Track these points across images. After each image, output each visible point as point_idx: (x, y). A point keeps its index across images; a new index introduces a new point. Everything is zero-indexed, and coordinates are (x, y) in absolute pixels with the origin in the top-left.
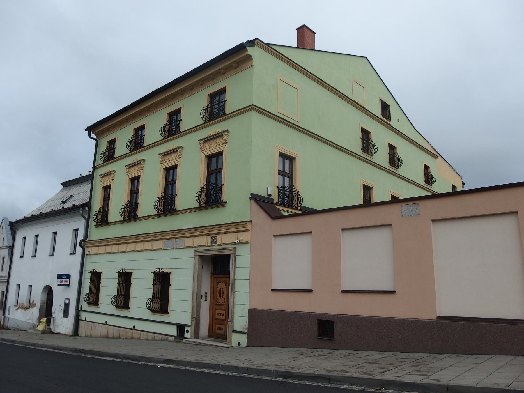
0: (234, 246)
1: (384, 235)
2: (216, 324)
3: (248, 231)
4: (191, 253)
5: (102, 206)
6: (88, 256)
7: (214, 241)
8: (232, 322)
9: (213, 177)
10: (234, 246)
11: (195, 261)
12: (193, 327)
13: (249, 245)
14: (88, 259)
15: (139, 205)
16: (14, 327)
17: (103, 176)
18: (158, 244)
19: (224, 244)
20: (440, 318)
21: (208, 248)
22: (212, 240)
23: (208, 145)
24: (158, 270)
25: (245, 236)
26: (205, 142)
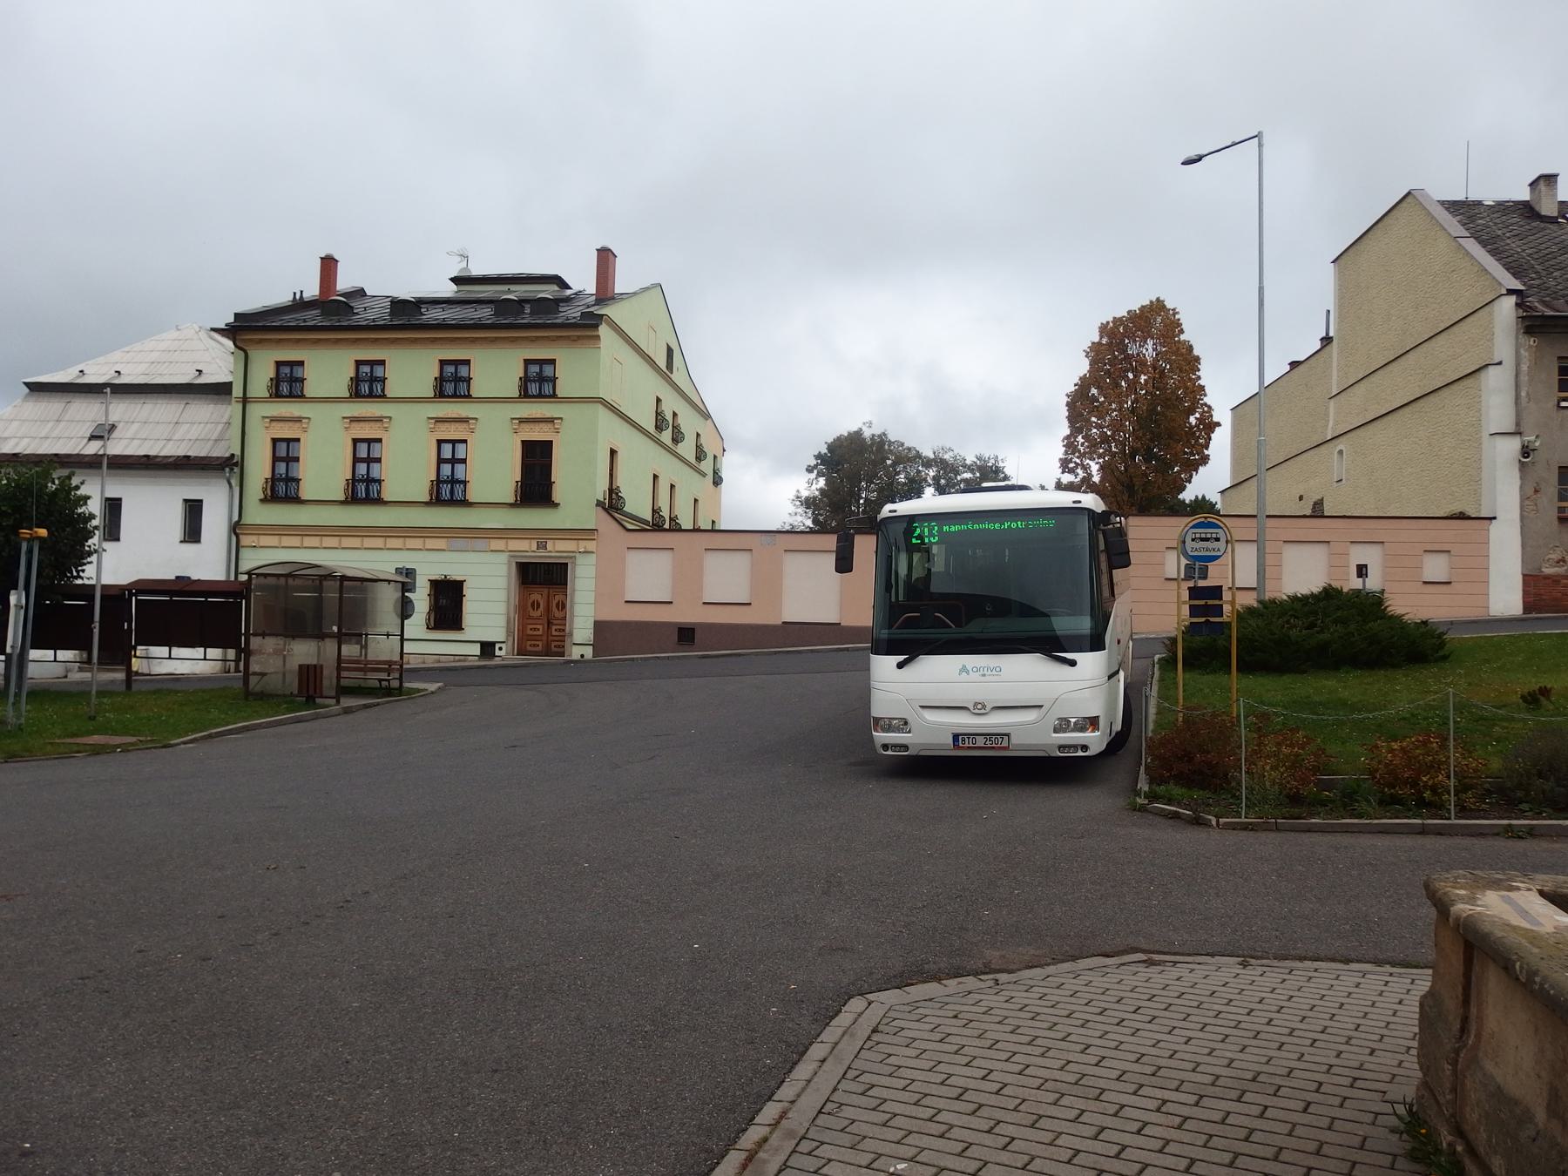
0: (574, 554)
1: (745, 557)
2: (541, 635)
3: (594, 539)
4: (503, 558)
5: (435, 479)
6: (244, 549)
7: (542, 546)
8: (571, 634)
9: (281, 468)
10: (574, 554)
11: (509, 569)
12: (510, 643)
13: (594, 555)
14: (244, 553)
15: (554, 485)
16: (1497, 917)
17: (351, 421)
18: (441, 543)
19: (557, 552)
20: (784, 623)
21: (533, 554)
22: (538, 545)
23: (526, 426)
24: (443, 577)
25: (591, 546)
26: (351, 421)
